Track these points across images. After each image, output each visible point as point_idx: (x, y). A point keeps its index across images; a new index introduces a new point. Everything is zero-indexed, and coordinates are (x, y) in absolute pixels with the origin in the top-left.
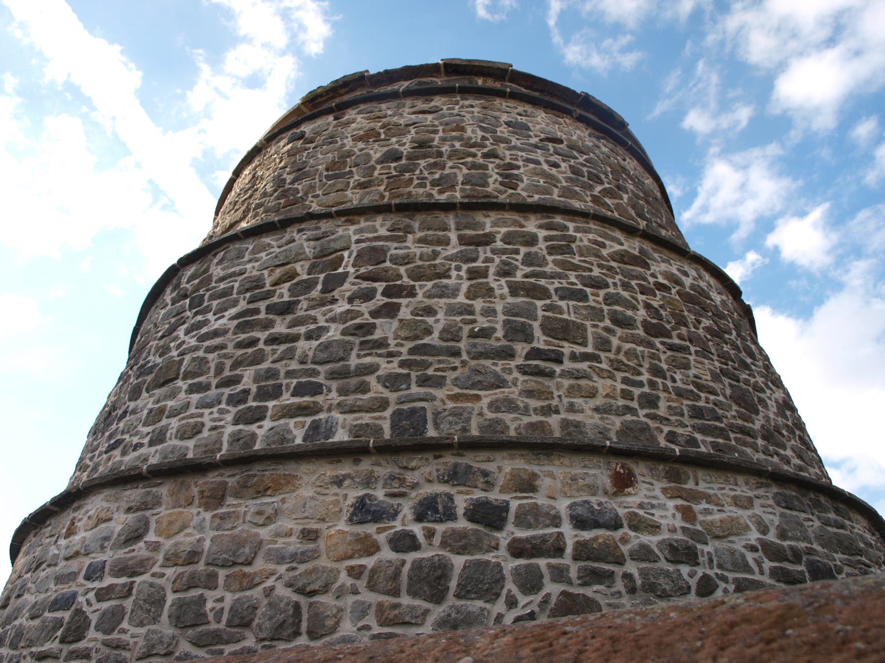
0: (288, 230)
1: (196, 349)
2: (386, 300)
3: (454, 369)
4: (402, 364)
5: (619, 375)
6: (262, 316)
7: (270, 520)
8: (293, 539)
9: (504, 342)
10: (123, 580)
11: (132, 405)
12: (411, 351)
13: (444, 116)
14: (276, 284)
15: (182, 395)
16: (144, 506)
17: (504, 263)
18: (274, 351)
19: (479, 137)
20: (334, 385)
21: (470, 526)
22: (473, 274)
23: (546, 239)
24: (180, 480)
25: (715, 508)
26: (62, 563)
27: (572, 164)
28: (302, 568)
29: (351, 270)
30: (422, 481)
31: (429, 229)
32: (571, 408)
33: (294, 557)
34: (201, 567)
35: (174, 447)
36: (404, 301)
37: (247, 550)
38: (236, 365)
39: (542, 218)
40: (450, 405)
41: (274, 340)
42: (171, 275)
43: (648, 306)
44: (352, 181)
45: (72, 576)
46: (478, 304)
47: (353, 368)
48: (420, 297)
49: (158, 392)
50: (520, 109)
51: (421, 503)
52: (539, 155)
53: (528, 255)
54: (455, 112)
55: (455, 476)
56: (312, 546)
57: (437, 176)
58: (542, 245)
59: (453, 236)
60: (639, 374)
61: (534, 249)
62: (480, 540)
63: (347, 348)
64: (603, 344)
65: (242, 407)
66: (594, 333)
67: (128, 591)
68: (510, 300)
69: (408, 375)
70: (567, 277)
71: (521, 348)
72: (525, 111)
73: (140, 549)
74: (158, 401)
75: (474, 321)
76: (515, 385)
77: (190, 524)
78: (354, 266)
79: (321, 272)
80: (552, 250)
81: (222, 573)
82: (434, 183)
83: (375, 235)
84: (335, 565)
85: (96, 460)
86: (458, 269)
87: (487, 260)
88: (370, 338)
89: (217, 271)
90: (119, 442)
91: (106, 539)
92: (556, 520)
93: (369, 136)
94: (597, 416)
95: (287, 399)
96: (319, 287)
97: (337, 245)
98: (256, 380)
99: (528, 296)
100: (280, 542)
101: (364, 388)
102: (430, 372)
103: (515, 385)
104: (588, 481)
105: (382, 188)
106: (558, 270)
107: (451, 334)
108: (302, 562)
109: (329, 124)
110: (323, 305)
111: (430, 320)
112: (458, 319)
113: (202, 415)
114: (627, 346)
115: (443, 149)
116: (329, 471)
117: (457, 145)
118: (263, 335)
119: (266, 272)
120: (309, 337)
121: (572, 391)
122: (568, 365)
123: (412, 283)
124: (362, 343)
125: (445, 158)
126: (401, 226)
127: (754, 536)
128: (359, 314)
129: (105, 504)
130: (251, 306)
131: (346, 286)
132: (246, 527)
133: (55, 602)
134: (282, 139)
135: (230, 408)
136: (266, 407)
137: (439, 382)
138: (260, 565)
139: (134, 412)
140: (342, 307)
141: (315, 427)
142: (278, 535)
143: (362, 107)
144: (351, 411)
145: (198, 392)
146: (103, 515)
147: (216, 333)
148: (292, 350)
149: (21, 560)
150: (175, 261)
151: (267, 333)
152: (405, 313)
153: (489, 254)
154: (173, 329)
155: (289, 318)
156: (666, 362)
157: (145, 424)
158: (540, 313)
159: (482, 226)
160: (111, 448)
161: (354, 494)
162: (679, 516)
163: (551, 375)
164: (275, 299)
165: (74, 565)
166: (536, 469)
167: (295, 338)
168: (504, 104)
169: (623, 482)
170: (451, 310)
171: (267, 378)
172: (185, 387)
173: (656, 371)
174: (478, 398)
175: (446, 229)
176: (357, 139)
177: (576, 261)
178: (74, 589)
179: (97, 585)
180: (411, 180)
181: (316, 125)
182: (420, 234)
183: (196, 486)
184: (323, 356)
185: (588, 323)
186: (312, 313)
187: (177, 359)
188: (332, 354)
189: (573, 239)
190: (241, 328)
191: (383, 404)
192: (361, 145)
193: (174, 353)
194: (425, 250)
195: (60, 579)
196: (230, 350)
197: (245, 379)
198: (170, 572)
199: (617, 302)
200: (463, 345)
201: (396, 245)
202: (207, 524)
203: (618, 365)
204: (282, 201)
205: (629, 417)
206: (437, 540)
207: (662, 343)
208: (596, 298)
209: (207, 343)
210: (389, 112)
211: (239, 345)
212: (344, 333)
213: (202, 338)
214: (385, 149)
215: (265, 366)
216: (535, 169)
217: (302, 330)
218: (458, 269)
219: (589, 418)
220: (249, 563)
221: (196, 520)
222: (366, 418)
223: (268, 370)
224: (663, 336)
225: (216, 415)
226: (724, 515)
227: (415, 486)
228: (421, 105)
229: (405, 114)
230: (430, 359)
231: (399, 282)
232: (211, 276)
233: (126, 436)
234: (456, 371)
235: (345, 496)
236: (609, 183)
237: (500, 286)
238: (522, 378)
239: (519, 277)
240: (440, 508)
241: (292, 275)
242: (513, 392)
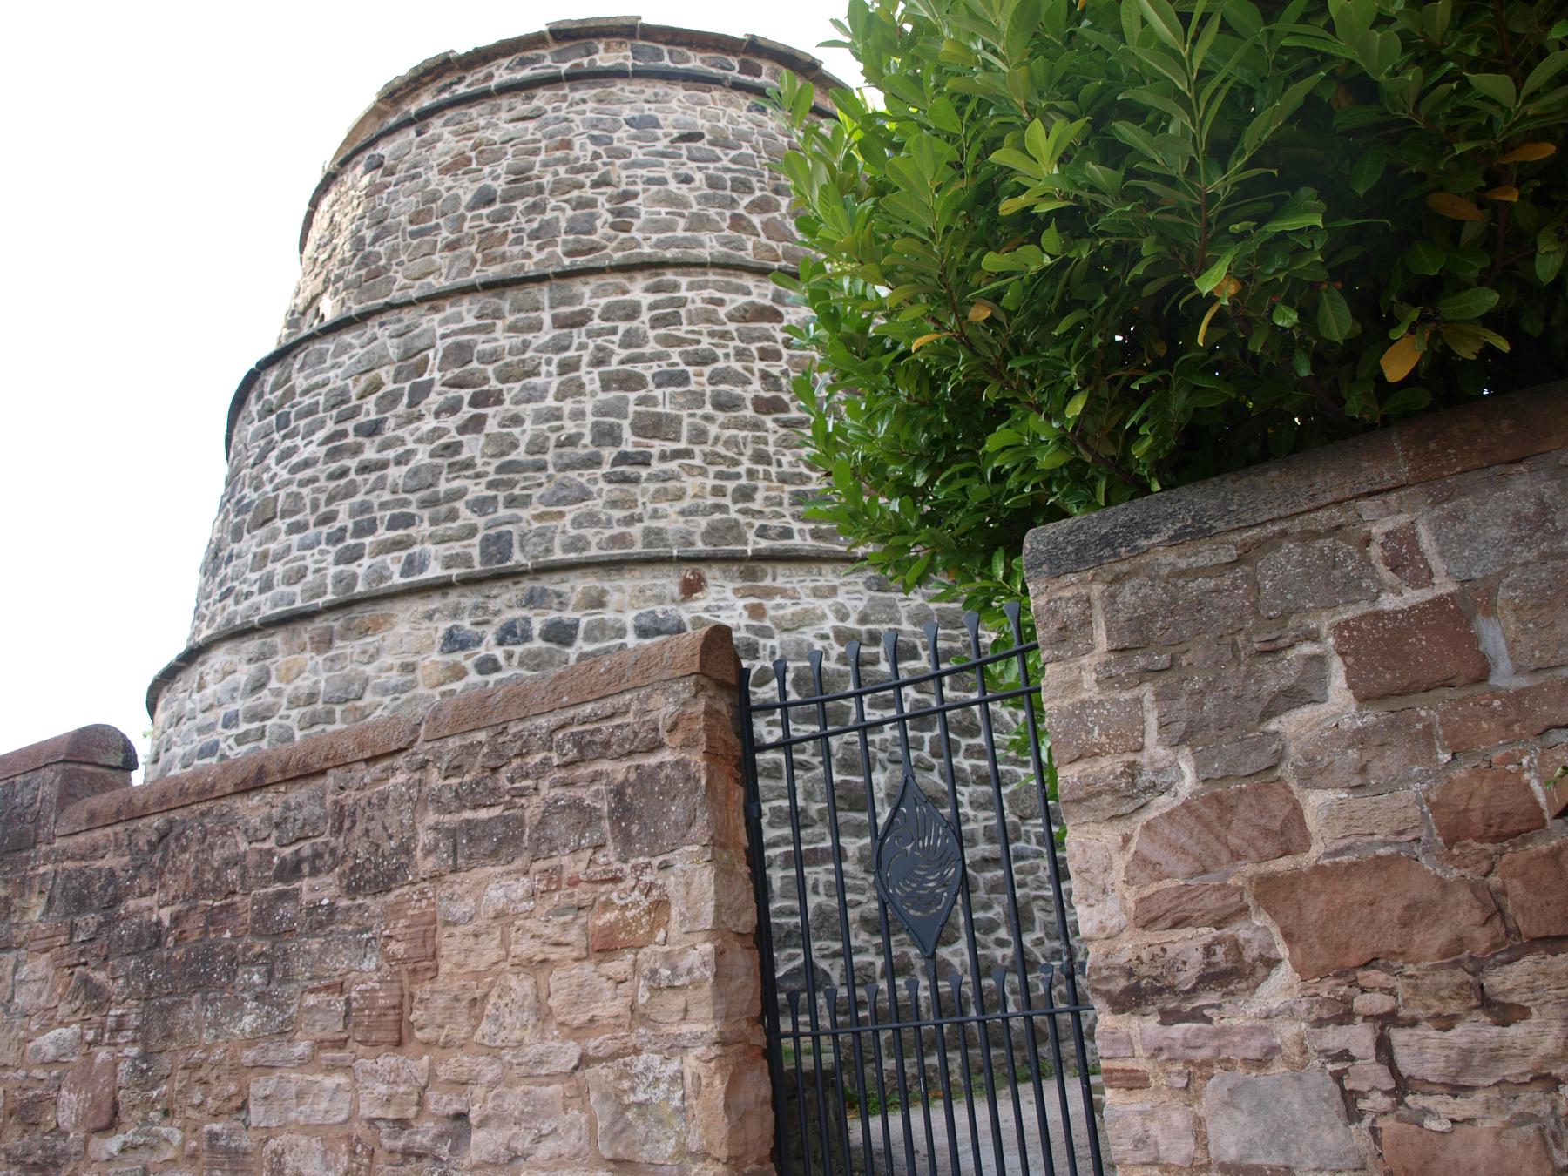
0: (370, 323)
1: (289, 483)
2: (474, 411)
3: (540, 485)
4: (490, 485)
5: (712, 470)
6: (351, 439)
7: (372, 658)
8: (394, 672)
9: (592, 449)
10: (256, 725)
11: (236, 547)
12: (499, 470)
13: (547, 124)
14: (362, 397)
15: (282, 537)
16: (262, 656)
17: (599, 349)
18: (366, 480)
19: (590, 154)
20: (426, 513)
21: (545, 645)
22: (567, 367)
23: (652, 307)
24: (291, 628)
25: (789, 602)
26: (200, 716)
27: (711, 172)
28: (404, 697)
29: (437, 375)
30: (504, 608)
31: (519, 311)
32: (655, 515)
33: (396, 689)
34: (320, 706)
35: (283, 594)
36: (490, 411)
37: (356, 687)
38: (331, 499)
39: (651, 276)
40: (535, 525)
41: (364, 469)
42: (251, 380)
43: (765, 376)
44: (439, 238)
45: (211, 727)
46: (567, 406)
47: (442, 495)
48: (507, 405)
49: (260, 533)
50: (649, 92)
51: (502, 629)
52: (666, 170)
53: (628, 332)
54: (562, 114)
55: (531, 601)
56: (410, 677)
57: (535, 225)
58: (645, 316)
59: (546, 317)
60: (737, 463)
61: (635, 324)
62: (552, 657)
63: (435, 472)
64: (699, 436)
65: (340, 546)
66: (690, 424)
67: (262, 734)
68: (602, 396)
69: (495, 497)
70: (668, 356)
71: (609, 453)
72: (656, 95)
73: (265, 696)
74: (260, 544)
75: (561, 428)
76: (600, 496)
77: (303, 669)
78: (440, 370)
79: (407, 380)
80: (656, 322)
81: (338, 709)
82: (534, 236)
83: (461, 325)
84: (431, 692)
85: (212, 609)
86: (549, 362)
87: (582, 347)
88: (457, 458)
89: (299, 381)
90: (230, 590)
91: (235, 690)
92: (621, 632)
93: (458, 164)
94: (681, 519)
95: (383, 534)
96: (405, 400)
97: (421, 344)
98: (352, 515)
99: (621, 388)
100: (384, 677)
101: (453, 516)
102: (516, 491)
103: (600, 496)
104: (656, 591)
105: (474, 248)
106: (660, 348)
107: (538, 446)
108: (403, 692)
109: (411, 143)
110: (410, 422)
111: (516, 431)
112: (545, 426)
113: (303, 558)
114: (727, 433)
115: (544, 181)
116: (420, 606)
117: (562, 170)
118: (352, 463)
119: (350, 382)
120: (399, 462)
121: (658, 496)
122: (656, 466)
123: (500, 386)
124: (450, 465)
125: (546, 195)
126: (489, 311)
127: (828, 626)
128: (445, 431)
129: (228, 658)
130: (340, 427)
131: (433, 397)
132: (354, 666)
133: (201, 751)
134: (357, 163)
135: (329, 548)
136: (363, 545)
137: (524, 502)
138: (369, 698)
139: (239, 556)
140: (428, 424)
141: (410, 561)
142: (381, 670)
143: (449, 114)
144: (442, 542)
145: (297, 532)
146: (227, 668)
147: (307, 464)
148: (382, 479)
149: (161, 716)
150: (253, 365)
151: (357, 460)
152: (492, 426)
153: (584, 339)
154: (262, 457)
155: (378, 439)
156: (776, 444)
157: (253, 570)
158: (632, 408)
159: (576, 299)
160: (224, 596)
161: (444, 626)
162: (746, 614)
163: (636, 480)
164: (362, 419)
165: (211, 717)
166: (607, 585)
167: (383, 465)
168: (627, 88)
169: (691, 588)
170: (540, 417)
171: (362, 513)
172: (284, 528)
173: (761, 458)
174: (561, 515)
175: (538, 309)
176: (445, 170)
177: (681, 334)
178: (215, 737)
179: (234, 731)
180: (506, 233)
181: (395, 144)
182: (510, 319)
183: (307, 631)
184: (413, 483)
185: (684, 413)
186: (400, 433)
187: (272, 495)
188: (421, 480)
189: (683, 302)
190: (333, 455)
191: (472, 531)
192: (448, 180)
193: (268, 488)
194: (514, 341)
195: (201, 730)
196: (322, 483)
197: (341, 516)
198: (295, 713)
199: (723, 381)
200: (549, 457)
201: (483, 337)
202: (320, 667)
203: (712, 458)
204: (363, 272)
205: (717, 516)
206: (515, 661)
207: (776, 421)
208: (699, 379)
209: (299, 476)
210: (482, 122)
211: (331, 477)
212: (432, 455)
213: (295, 469)
214: (477, 185)
215: (358, 498)
216: (658, 192)
217: (390, 454)
218: (549, 362)
219: (672, 523)
220: (360, 698)
221: (310, 664)
222: (456, 548)
223: (362, 503)
224: (777, 411)
225: (317, 557)
226: (798, 608)
227: (497, 613)
228: (522, 108)
229: (502, 124)
230: (517, 477)
231: (485, 388)
232: (293, 388)
233: (236, 583)
234: (540, 487)
235: (436, 629)
236: (762, 189)
237: (590, 377)
238: (606, 487)
239: (614, 366)
240: (518, 631)
241: (376, 386)
242: (595, 505)
